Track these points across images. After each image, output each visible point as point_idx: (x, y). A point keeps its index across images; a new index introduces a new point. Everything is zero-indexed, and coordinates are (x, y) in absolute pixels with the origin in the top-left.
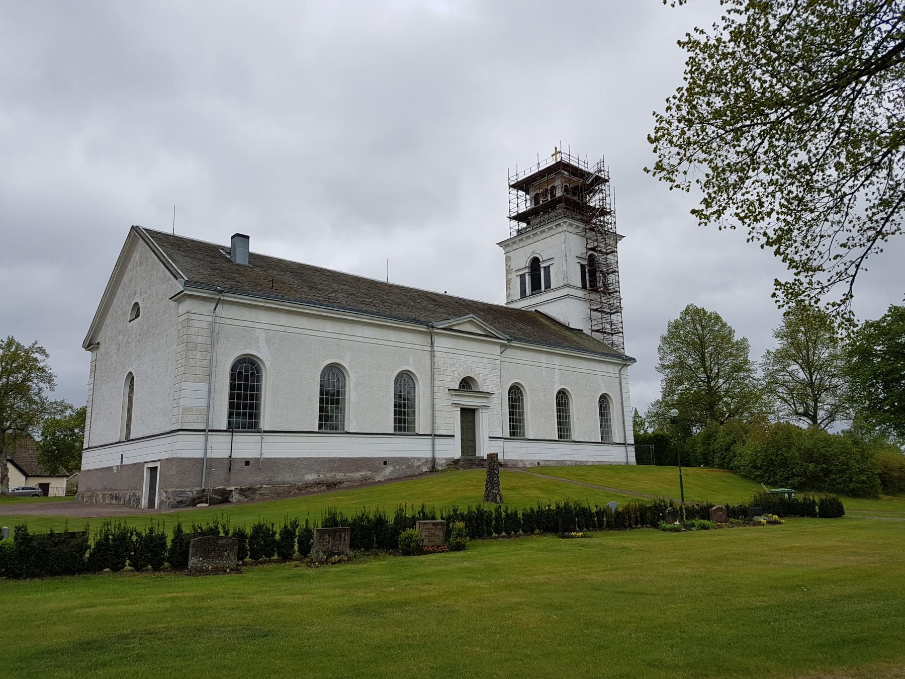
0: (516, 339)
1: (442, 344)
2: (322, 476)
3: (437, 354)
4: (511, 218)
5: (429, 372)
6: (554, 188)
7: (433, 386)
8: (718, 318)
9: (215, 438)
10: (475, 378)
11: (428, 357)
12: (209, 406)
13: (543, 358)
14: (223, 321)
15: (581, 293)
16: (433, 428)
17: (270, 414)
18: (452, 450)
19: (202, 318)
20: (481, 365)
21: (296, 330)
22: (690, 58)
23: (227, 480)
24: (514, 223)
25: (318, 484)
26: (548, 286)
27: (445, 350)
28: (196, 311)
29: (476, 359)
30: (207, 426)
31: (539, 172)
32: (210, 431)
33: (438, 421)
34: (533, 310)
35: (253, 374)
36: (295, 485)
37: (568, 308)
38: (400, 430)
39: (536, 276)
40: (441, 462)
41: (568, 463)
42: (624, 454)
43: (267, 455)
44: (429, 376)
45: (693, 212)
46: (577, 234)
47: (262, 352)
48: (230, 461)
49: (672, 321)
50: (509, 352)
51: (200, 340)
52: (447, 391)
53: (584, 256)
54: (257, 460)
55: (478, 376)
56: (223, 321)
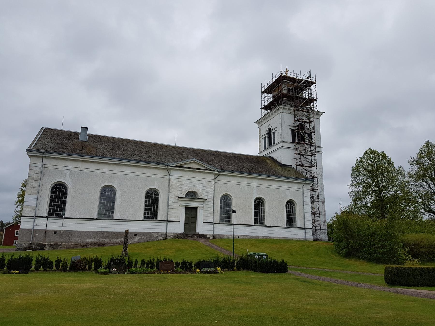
0: (222, 171)
1: (175, 174)
2: (96, 240)
3: (171, 179)
4: (262, 109)
5: (167, 189)
6: (282, 90)
7: (169, 196)
8: (384, 155)
9: (39, 220)
10: (197, 192)
11: (167, 181)
12: (37, 205)
13: (246, 181)
14: (48, 166)
15: (291, 145)
16: (167, 218)
18: (180, 228)
19: (37, 165)
20: (201, 185)
21: (86, 170)
24: (263, 111)
25: (93, 244)
26: (274, 143)
27: (177, 177)
28: (34, 162)
29: (198, 182)
30: (35, 214)
31: (273, 83)
32: (36, 217)
33: (169, 214)
34: (268, 156)
35: (63, 191)
36: (80, 244)
37: (285, 155)
38: (148, 218)
39: (270, 138)
40: (170, 235)
41: (260, 238)
42: (304, 234)
43: (66, 229)
44: (167, 191)
45: (289, 94)
46: (290, 113)
47: (68, 181)
48: (46, 230)
49: (359, 159)
50: (221, 178)
51: (35, 175)
52: (177, 198)
53: (294, 125)
54: (60, 231)
55: (199, 191)
56: (48, 166)
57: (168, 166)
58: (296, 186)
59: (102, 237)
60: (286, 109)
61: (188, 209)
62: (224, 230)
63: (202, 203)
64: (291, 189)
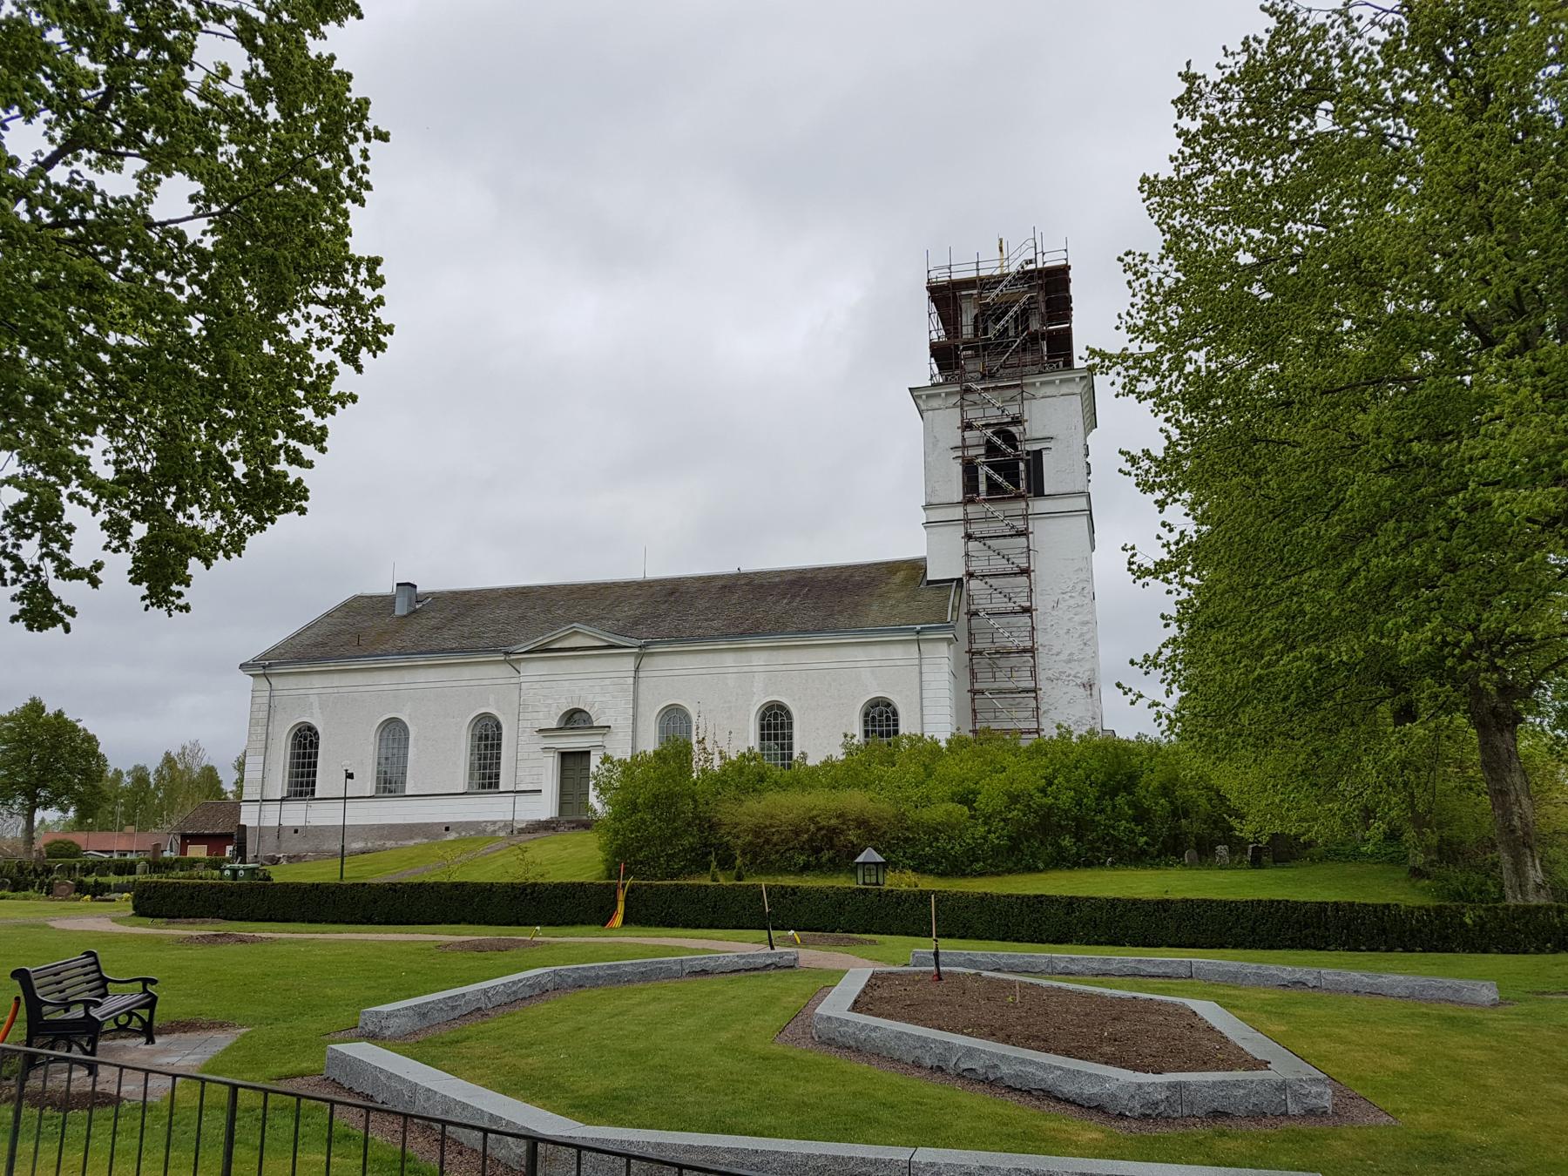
1: (534, 670)
13: (729, 659)
17: (327, 779)
18: (545, 807)
22: (1129, 388)
23: (278, 847)
29: (590, 683)
43: (315, 822)
57: (507, 653)
58: (897, 652)
59: (381, 837)
60: (1053, 382)
61: (565, 756)
62: (296, 814)
63: (600, 738)
64: (877, 663)
